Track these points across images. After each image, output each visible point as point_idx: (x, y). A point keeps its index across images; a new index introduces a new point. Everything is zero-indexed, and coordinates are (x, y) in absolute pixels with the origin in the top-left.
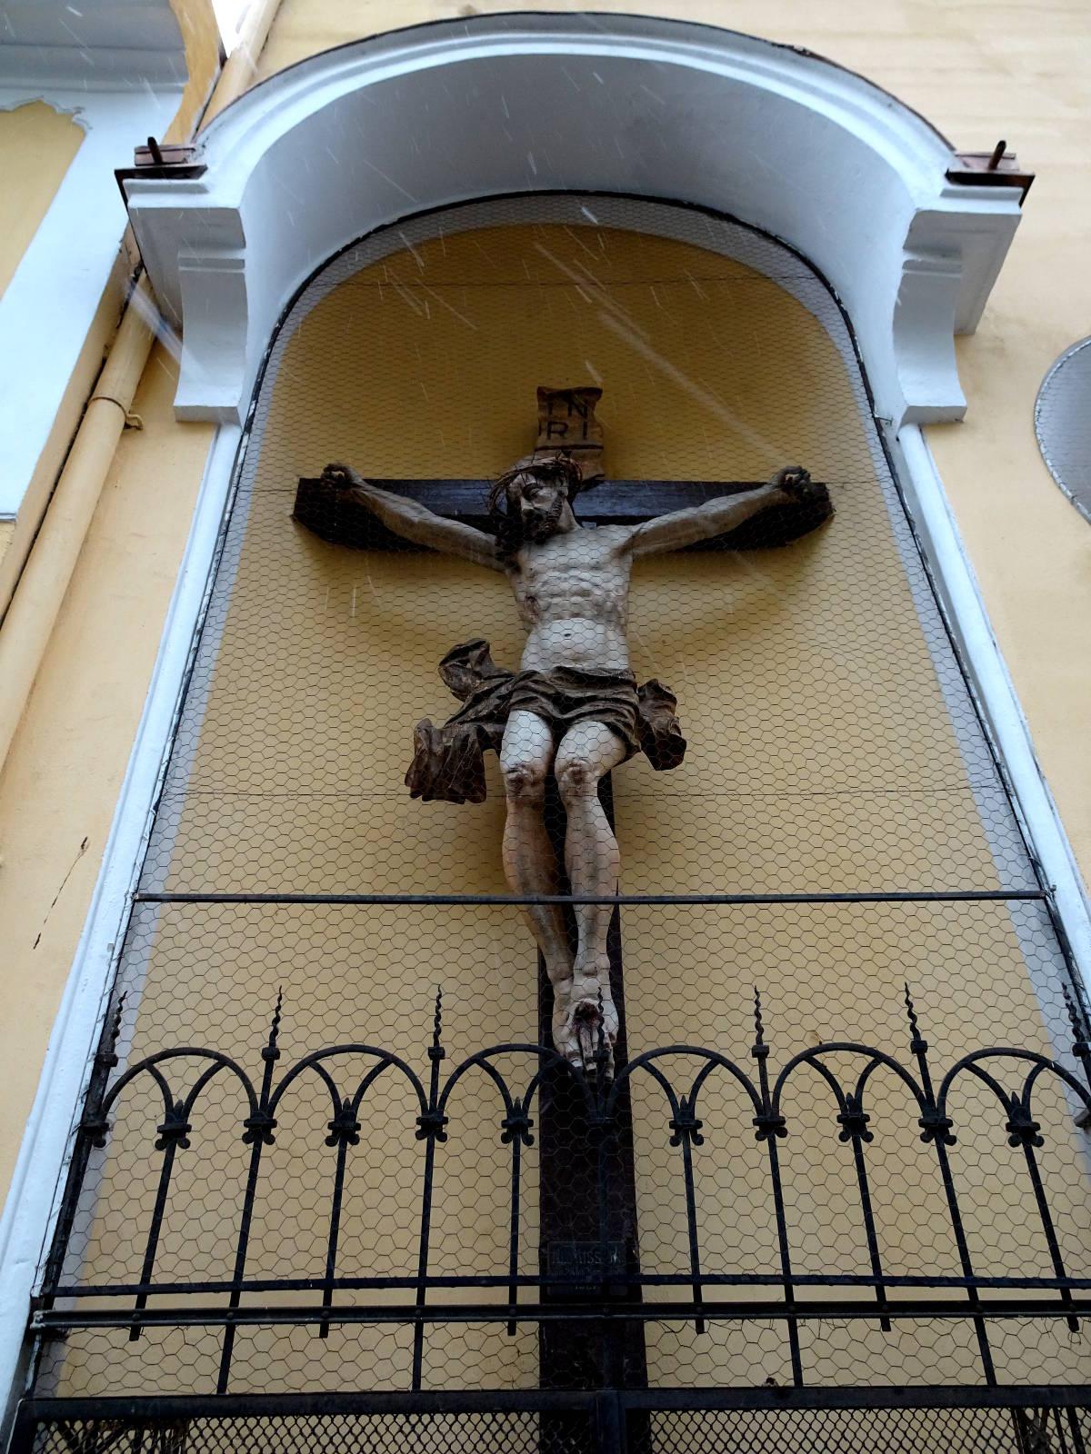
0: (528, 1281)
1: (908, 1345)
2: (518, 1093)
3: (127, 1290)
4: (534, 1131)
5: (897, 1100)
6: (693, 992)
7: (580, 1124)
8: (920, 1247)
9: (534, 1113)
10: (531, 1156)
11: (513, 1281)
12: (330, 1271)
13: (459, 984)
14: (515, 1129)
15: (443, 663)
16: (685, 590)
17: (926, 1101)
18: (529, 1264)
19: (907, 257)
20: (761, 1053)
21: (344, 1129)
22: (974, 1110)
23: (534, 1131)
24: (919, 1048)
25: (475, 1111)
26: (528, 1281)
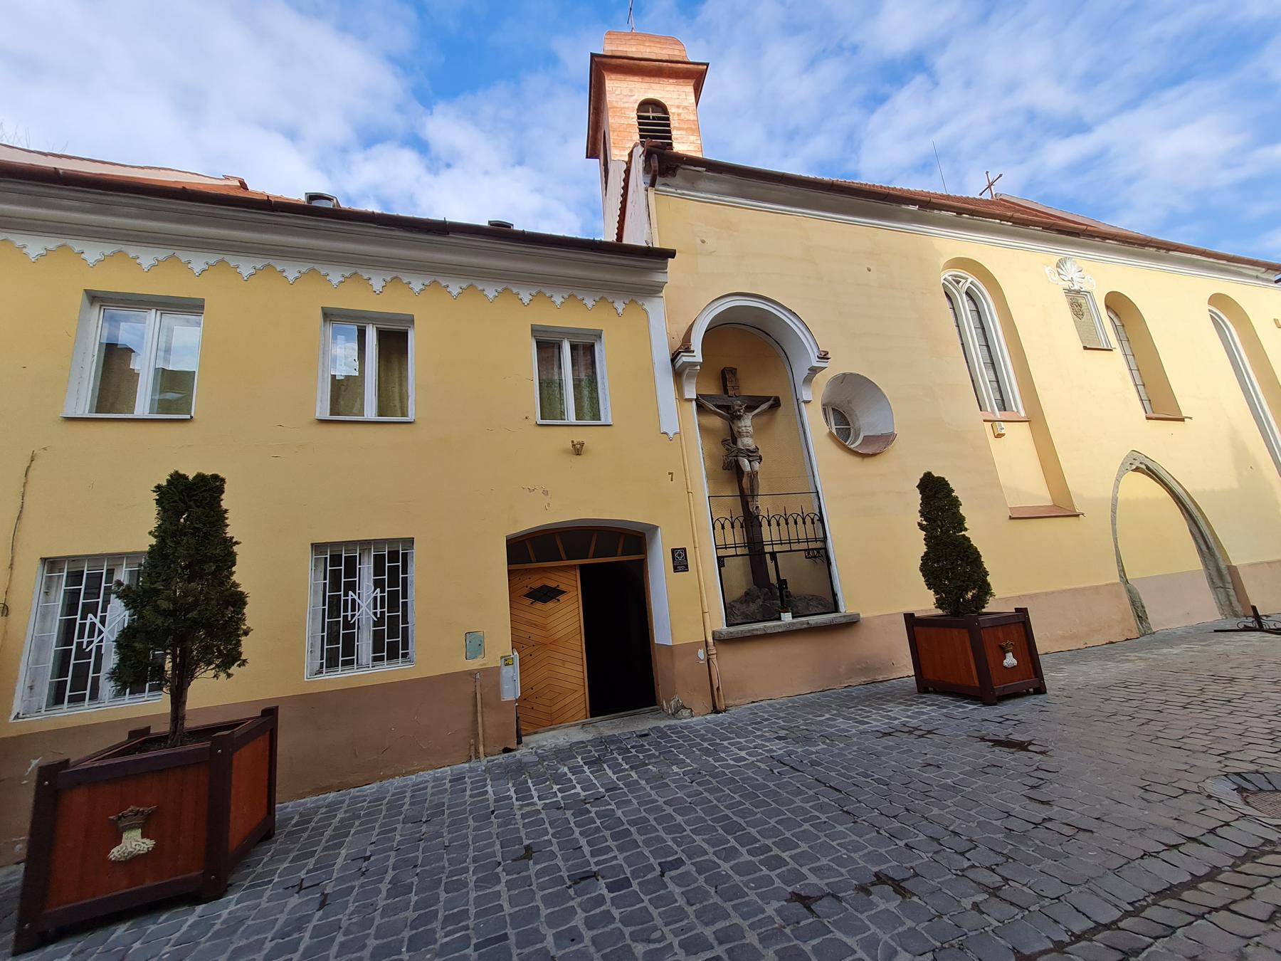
25: (737, 524)
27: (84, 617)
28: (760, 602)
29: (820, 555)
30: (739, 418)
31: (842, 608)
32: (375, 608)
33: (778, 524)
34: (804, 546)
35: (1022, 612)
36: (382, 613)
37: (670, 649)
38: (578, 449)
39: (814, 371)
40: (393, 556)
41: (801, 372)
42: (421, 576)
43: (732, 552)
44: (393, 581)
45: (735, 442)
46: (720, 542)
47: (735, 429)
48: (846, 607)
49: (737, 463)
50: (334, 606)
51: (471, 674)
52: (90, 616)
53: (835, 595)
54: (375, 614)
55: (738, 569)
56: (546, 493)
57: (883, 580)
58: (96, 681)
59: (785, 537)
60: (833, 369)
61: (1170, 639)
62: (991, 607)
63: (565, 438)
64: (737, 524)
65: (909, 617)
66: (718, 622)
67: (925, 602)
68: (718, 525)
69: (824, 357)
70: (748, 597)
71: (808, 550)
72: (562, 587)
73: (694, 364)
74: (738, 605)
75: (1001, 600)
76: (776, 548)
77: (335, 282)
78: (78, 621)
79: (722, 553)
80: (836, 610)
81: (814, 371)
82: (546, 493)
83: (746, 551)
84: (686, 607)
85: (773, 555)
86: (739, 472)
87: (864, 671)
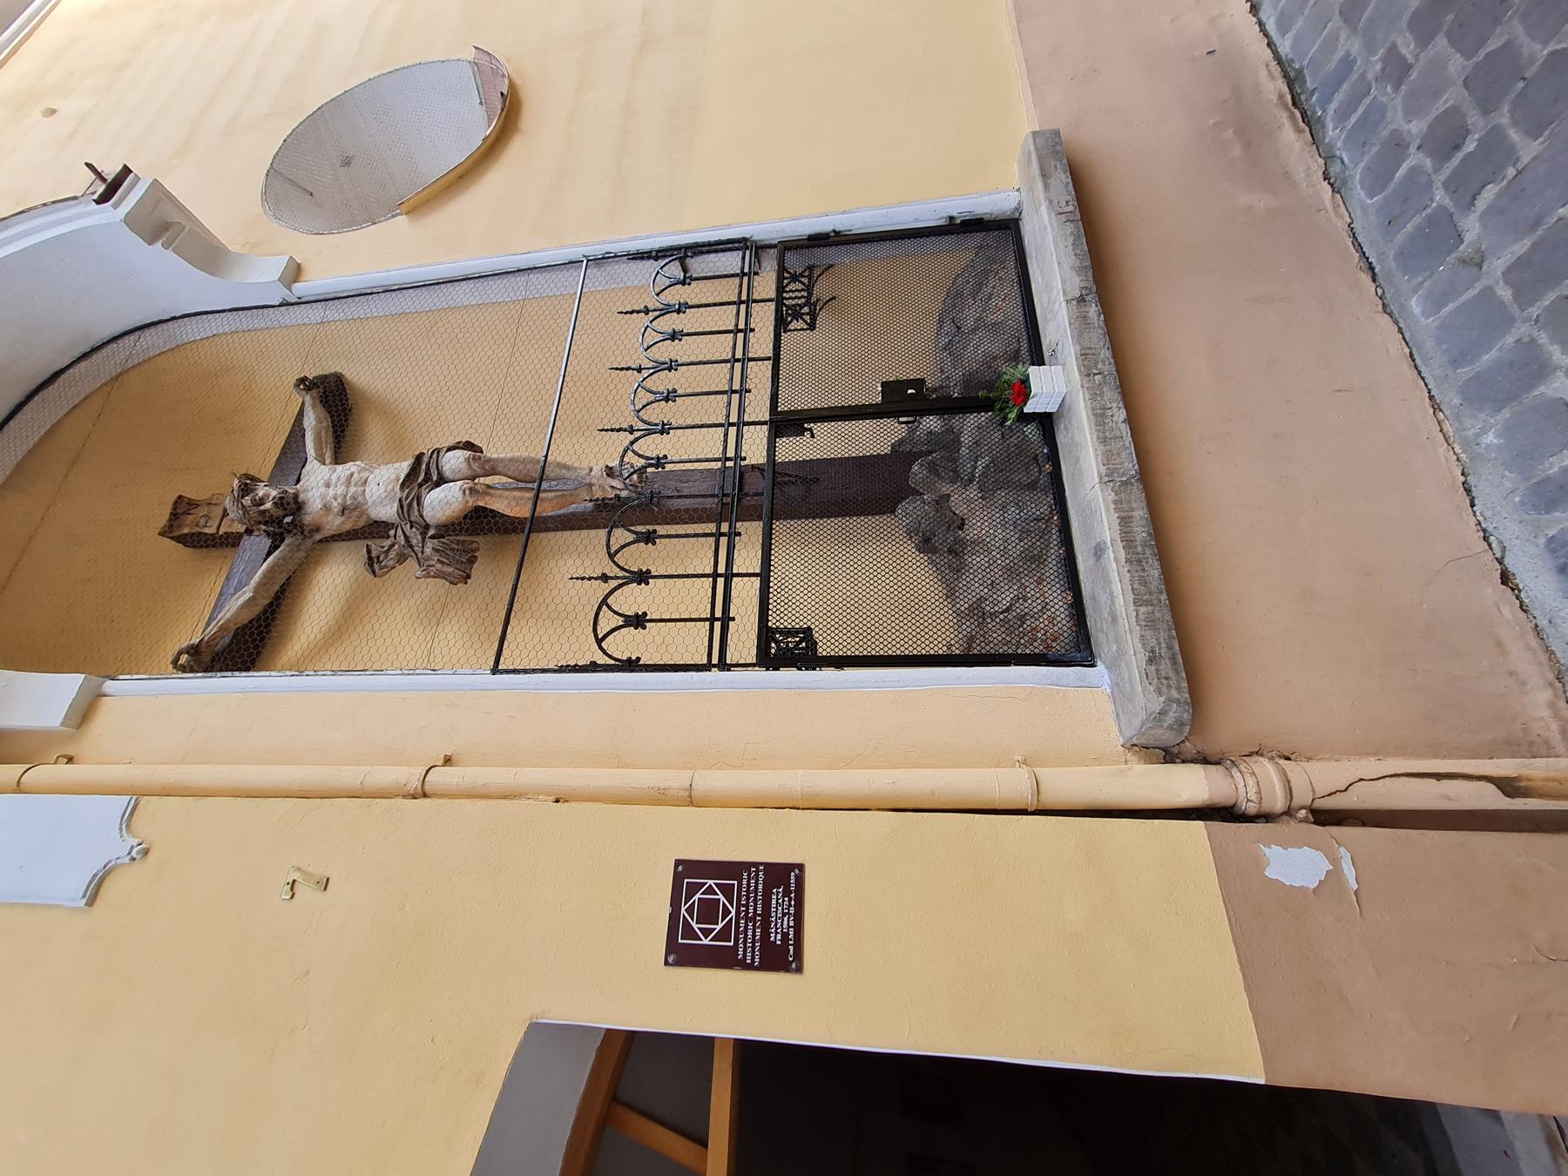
0: (719, 528)
1: (756, 381)
2: (631, 537)
3: (716, 460)
4: (651, 528)
5: (658, 411)
6: (592, 457)
7: (640, 507)
8: (696, 598)
9: (641, 528)
10: (661, 530)
11: (718, 535)
12: (755, 301)
13: (571, 567)
14: (649, 538)
15: (374, 572)
16: (310, 596)
17: (649, 433)
18: (711, 528)
19: (158, 245)
20: (605, 578)
21: (638, 621)
22: (657, 413)
23: (651, 528)
24: (647, 311)
25: (638, 557)
26: (719, 528)
28: (962, 500)
29: (804, 272)
33: (670, 396)
34: (764, 318)
43: (745, 593)
45: (378, 529)
46: (692, 643)
47: (335, 523)
48: (1000, 182)
49: (447, 529)
55: (834, 574)
59: (725, 318)
64: (638, 557)
66: (1076, 721)
68: (625, 644)
70: (942, 543)
74: (973, 588)
76: (758, 407)
79: (743, 643)
83: (751, 532)
85: (785, 424)
86: (478, 522)
87: (1247, 131)
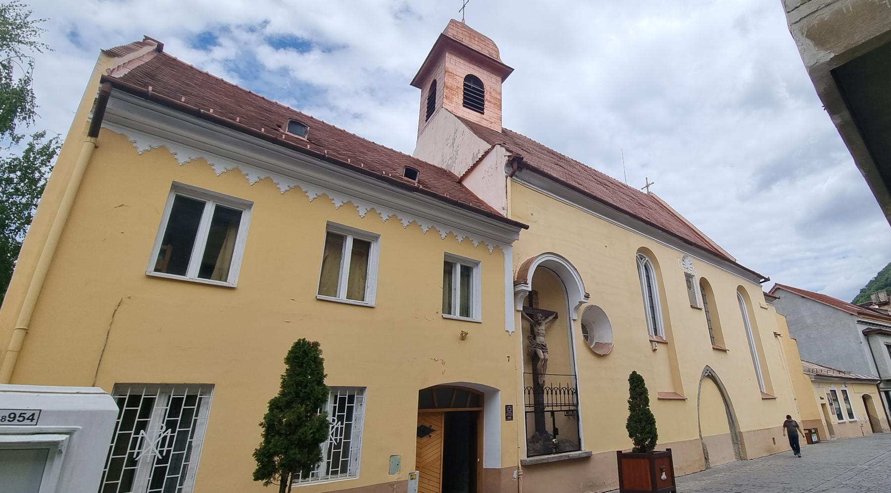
27: (137, 433)
29: (573, 414)
30: (540, 324)
31: (583, 448)
32: (163, 446)
34: (567, 408)
35: (669, 450)
36: (341, 439)
37: (498, 471)
38: (463, 337)
39: (581, 303)
40: (191, 399)
41: (573, 303)
42: (361, 413)
44: (186, 422)
45: (535, 338)
47: (536, 330)
48: (585, 448)
50: (121, 443)
51: (391, 485)
52: (142, 431)
53: (580, 440)
54: (161, 452)
56: (443, 363)
57: (605, 433)
58: (329, 458)
60: (590, 302)
61: (717, 471)
62: (656, 449)
63: (458, 328)
65: (619, 453)
67: (628, 445)
69: (587, 296)
71: (567, 411)
72: (433, 428)
73: (526, 291)
75: (660, 446)
76: (555, 409)
77: (337, 205)
78: (132, 436)
80: (580, 449)
81: (581, 303)
82: (443, 363)
84: (503, 442)
85: (552, 412)
